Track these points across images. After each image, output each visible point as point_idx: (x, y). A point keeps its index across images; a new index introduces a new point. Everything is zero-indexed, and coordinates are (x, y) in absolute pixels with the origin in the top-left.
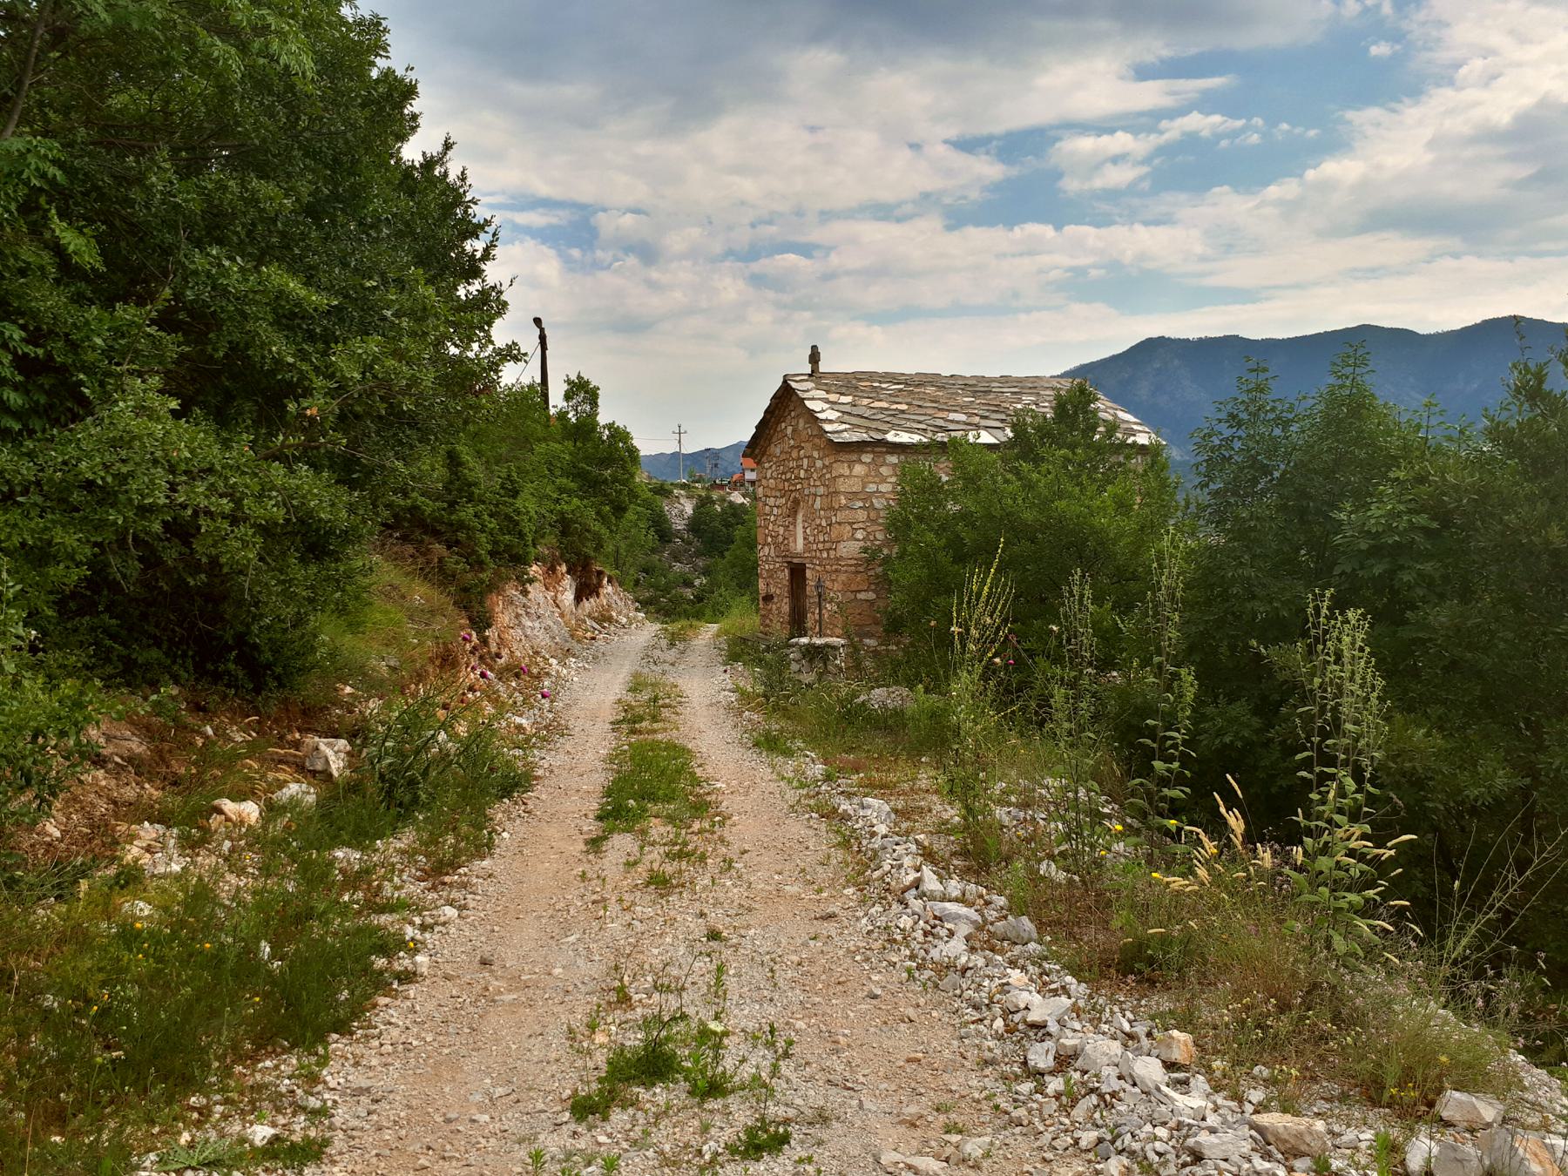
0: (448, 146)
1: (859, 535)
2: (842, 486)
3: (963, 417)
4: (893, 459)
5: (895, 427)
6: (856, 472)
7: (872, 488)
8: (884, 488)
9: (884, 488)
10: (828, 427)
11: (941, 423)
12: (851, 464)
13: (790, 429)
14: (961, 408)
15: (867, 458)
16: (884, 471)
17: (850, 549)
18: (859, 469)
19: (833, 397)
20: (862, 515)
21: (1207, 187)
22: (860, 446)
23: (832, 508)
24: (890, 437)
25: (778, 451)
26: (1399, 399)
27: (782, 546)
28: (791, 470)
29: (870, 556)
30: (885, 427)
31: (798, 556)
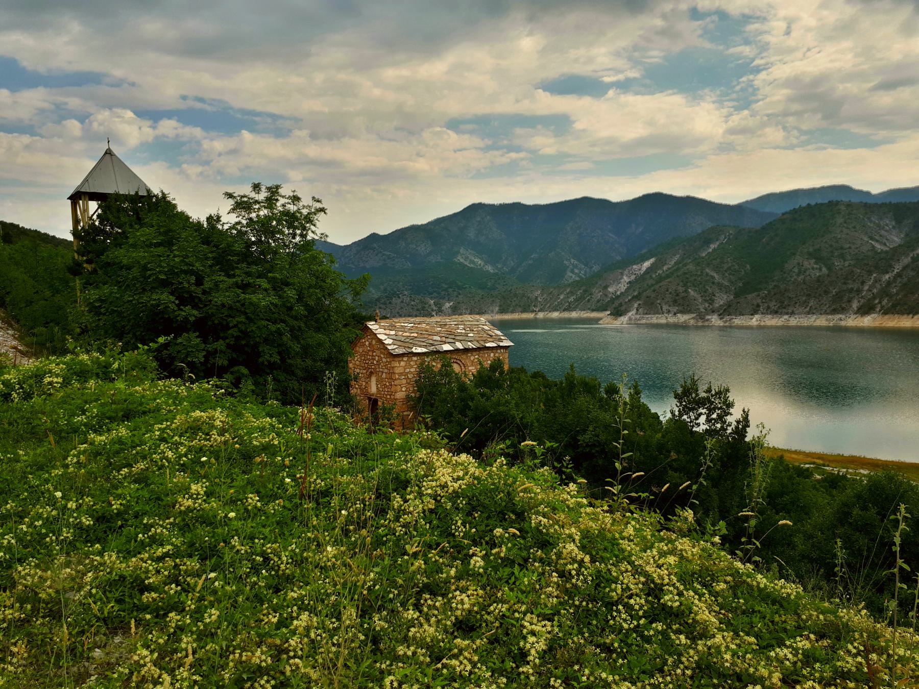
0: (230, 196)
1: (404, 389)
2: (397, 371)
3: (439, 338)
4: (415, 358)
5: (415, 345)
6: (400, 366)
7: (408, 370)
8: (413, 370)
9: (413, 370)
10: (389, 347)
11: (431, 342)
12: (399, 362)
13: (367, 343)
14: (437, 334)
15: (405, 359)
16: (412, 363)
17: (400, 395)
18: (402, 364)
19: (387, 332)
20: (404, 381)
21: (37, 87)
22: (403, 355)
23: (391, 379)
24: (414, 350)
25: (361, 350)
26: (787, 456)
27: (365, 391)
28: (369, 360)
29: (408, 398)
30: (411, 346)
31: (373, 395)
